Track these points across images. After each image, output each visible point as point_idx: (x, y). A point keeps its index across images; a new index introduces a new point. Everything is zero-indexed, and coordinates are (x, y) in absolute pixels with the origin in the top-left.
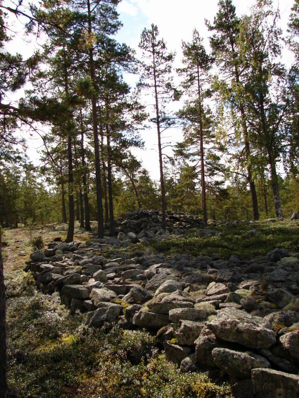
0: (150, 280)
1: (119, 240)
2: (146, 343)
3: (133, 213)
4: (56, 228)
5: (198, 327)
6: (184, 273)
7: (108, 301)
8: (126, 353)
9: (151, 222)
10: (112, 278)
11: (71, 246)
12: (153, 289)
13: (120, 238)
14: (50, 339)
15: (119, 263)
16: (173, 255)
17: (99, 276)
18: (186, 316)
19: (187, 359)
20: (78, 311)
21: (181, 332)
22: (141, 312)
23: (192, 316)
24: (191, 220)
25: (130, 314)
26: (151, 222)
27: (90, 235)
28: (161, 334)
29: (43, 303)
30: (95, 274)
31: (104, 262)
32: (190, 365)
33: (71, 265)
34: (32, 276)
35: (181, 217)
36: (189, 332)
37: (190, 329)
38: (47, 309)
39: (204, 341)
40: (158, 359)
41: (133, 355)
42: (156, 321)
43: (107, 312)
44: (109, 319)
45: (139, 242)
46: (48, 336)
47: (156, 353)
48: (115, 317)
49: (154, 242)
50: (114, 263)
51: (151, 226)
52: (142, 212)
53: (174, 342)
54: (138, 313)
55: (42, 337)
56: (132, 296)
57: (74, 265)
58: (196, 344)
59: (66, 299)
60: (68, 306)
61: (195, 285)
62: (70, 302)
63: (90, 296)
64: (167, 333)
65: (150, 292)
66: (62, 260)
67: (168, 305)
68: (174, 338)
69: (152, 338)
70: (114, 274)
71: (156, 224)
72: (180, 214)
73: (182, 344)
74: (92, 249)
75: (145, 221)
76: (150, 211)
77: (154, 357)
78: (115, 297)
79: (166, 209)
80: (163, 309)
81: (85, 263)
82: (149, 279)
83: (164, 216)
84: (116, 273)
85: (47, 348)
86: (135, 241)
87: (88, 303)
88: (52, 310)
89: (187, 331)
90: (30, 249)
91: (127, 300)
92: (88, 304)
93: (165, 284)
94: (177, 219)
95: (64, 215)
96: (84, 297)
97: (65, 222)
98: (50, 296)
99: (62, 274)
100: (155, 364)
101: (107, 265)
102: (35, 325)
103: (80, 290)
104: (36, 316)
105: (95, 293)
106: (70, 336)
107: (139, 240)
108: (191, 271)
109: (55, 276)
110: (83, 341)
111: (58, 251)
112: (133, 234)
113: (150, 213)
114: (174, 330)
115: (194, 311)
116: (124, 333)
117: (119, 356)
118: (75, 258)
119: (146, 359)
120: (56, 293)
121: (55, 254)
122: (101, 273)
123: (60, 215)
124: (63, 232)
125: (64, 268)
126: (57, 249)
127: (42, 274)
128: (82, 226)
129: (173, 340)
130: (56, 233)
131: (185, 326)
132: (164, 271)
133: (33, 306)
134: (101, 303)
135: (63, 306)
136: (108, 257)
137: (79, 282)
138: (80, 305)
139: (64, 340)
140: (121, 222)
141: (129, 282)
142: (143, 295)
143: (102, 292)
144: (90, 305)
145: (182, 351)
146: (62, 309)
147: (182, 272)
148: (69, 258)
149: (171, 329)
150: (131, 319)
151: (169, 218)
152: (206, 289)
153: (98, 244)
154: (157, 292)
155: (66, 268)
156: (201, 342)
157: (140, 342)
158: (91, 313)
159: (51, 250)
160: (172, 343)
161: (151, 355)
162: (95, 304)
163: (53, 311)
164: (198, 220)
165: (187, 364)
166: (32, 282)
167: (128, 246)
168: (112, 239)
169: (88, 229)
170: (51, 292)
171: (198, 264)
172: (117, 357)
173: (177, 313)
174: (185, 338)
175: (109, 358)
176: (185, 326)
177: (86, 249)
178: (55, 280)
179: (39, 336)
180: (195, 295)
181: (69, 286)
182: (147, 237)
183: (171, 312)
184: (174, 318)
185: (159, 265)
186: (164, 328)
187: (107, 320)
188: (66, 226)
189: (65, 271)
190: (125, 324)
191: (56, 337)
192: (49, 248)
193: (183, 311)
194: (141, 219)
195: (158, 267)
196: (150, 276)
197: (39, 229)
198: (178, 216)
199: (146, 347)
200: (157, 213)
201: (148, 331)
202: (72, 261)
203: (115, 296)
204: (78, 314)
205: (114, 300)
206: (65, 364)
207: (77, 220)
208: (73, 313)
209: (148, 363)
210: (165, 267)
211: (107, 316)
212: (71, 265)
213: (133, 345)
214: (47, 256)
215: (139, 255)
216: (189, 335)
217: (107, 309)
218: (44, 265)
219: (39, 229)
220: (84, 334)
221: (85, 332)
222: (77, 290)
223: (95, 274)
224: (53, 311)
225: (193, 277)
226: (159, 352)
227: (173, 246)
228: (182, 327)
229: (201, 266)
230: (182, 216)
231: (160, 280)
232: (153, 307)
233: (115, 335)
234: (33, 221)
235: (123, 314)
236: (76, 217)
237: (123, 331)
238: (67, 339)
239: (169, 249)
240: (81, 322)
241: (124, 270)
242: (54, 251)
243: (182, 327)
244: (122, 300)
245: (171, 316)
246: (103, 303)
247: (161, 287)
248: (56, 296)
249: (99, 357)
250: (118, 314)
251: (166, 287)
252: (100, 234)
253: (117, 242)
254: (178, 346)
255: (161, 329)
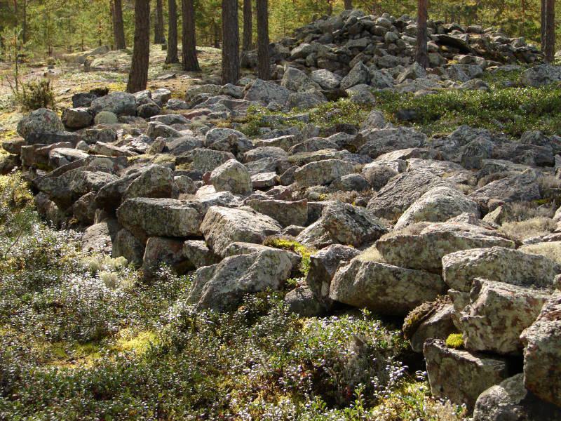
0: (382, 190)
1: (287, 92)
2: (370, 350)
3: (327, 23)
4: (95, 63)
5: (532, 301)
6: (483, 174)
7: (257, 240)
8: (308, 373)
9: (383, 51)
10: (264, 187)
11: (142, 101)
12: (391, 213)
13: (288, 85)
14: (82, 343)
15: (286, 150)
16: (449, 128)
17: (226, 178)
18: (495, 271)
19: (496, 391)
20: (165, 270)
21: (478, 312)
22: (358, 263)
23: (514, 273)
24: (503, 50)
25: (320, 272)
26: (383, 51)
27: (196, 83)
28: (417, 324)
29: (58, 253)
30: (217, 172)
31: (241, 145)
32: (503, 407)
33: (141, 153)
34: (25, 184)
35: (475, 41)
36: (501, 314)
37: (508, 304)
38: (76, 269)
39: (553, 332)
40: (405, 395)
41: (333, 379)
42: (400, 289)
43: (253, 266)
44: (257, 288)
45: (346, 96)
46: (76, 335)
47: (400, 377)
48: (277, 283)
49: (391, 98)
50: (271, 148)
51: (381, 63)
52: (354, 21)
53: (457, 343)
54: (349, 266)
55: (57, 339)
56: (327, 227)
57: (153, 152)
58: (525, 340)
59: (130, 242)
60: (136, 257)
61: (516, 207)
62: (140, 249)
63: (203, 228)
64: (435, 319)
65: (383, 222)
66: (117, 138)
67: (440, 242)
68: (456, 331)
69: (389, 338)
70: (274, 175)
71: (396, 58)
72: (470, 31)
73: (481, 347)
74: (205, 113)
75: (361, 49)
76: (380, 19)
77: (395, 388)
78: (277, 232)
79: (427, 17)
80: (424, 256)
81: (186, 146)
82: (377, 189)
83: (422, 35)
84: (278, 173)
85: (73, 367)
86: (335, 94)
87: (197, 248)
88: (85, 271)
89: (497, 309)
90: (14, 119)
91: (312, 240)
92: (195, 249)
93: (430, 197)
94: (460, 47)
95: (118, 25)
96: (184, 230)
97: (121, 45)
98: (78, 235)
99: (115, 171)
100: (397, 408)
101: (251, 153)
102: (37, 308)
103: (171, 211)
104: (37, 285)
105: (217, 218)
106: (142, 335)
107: (348, 91)
108: (506, 169)
109: (96, 178)
110: (180, 346)
111: (102, 113)
112: (330, 74)
113: (379, 24)
114: (457, 309)
115: (519, 258)
116: (301, 326)
117: (291, 382)
118: (155, 133)
119: (368, 392)
120: (98, 227)
121: (92, 123)
122: (235, 168)
123: (104, 30)
124: (115, 74)
125: (120, 160)
126: (100, 108)
127: (56, 174)
128: (172, 59)
129: (453, 339)
130: (93, 75)
131: (491, 293)
132: (421, 168)
133: (29, 261)
134: (237, 246)
135: (120, 261)
136: (255, 133)
137: (167, 192)
138: (171, 255)
139: (125, 344)
140: (291, 49)
141: (317, 194)
142: (361, 225)
143: (238, 216)
144: (202, 252)
145: (479, 368)
146: (117, 269)
147: (478, 173)
148: (135, 134)
149: (446, 309)
150: (324, 287)
151: (437, 43)
152: (552, 217)
153: (224, 98)
154: (403, 219)
155: (129, 158)
156: (542, 336)
157: (353, 343)
158: (206, 271)
159: (83, 109)
160: (450, 347)
161: (384, 382)
162: (216, 251)
163: (88, 274)
164: (525, 51)
165: (494, 404)
166: (24, 201)
167: (312, 107)
168: (266, 87)
169: (191, 65)
170: (84, 223)
171: (529, 152)
172: (282, 385)
173: (467, 260)
174: (489, 328)
175: (259, 390)
176: (491, 293)
177: (188, 113)
178: (96, 188)
179: (48, 335)
180: (518, 230)
181: (139, 200)
182: (369, 83)
183: (448, 261)
184: (457, 277)
185: (409, 151)
186: (425, 306)
187: (252, 290)
188: (124, 59)
189: (126, 166)
190: (306, 302)
191: (100, 338)
192: (74, 107)
193: (485, 255)
194: (350, 43)
195: (404, 158)
196: (380, 180)
197: (41, 66)
198: (462, 37)
199: (372, 358)
200: (400, 26)
201: (375, 319)
202: (145, 140)
203: (279, 230)
204: (165, 279)
205: (273, 238)
206: (128, 402)
207: (156, 42)
208: (149, 278)
209: (377, 403)
210: (426, 158)
211: (254, 277)
212: (141, 153)
213: (332, 354)
214: (68, 128)
215: (349, 130)
216: (503, 320)
217: (255, 258)
218: (59, 151)
219: (41, 66)
220: (184, 329)
221: (187, 324)
222: (166, 210)
223: (217, 172)
224: (88, 274)
225: (511, 183)
226: (410, 376)
227: (451, 109)
228: (483, 297)
229: (536, 158)
230: (476, 37)
231: (413, 189)
232: (393, 250)
233: (278, 329)
234: (25, 37)
235: (301, 275)
236: (152, 38)
237: (301, 321)
238: (133, 342)
239: (436, 117)
240: (174, 298)
241: (302, 163)
242: (93, 113)
243: (483, 297)
244: (298, 238)
245: (448, 269)
246: (241, 244)
247: (415, 207)
248: (98, 233)
249: (229, 388)
250: (285, 274)
251: (430, 204)
252: (230, 72)
253: (279, 96)
254: (467, 356)
255: (418, 309)
